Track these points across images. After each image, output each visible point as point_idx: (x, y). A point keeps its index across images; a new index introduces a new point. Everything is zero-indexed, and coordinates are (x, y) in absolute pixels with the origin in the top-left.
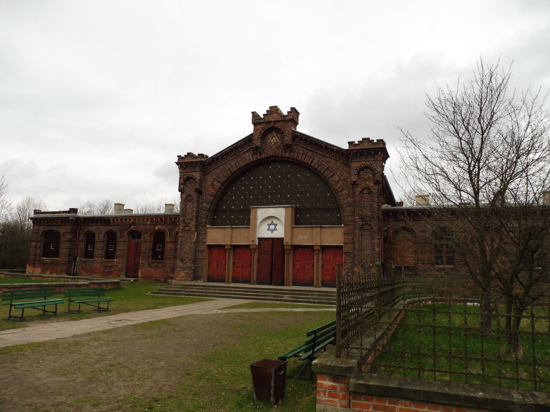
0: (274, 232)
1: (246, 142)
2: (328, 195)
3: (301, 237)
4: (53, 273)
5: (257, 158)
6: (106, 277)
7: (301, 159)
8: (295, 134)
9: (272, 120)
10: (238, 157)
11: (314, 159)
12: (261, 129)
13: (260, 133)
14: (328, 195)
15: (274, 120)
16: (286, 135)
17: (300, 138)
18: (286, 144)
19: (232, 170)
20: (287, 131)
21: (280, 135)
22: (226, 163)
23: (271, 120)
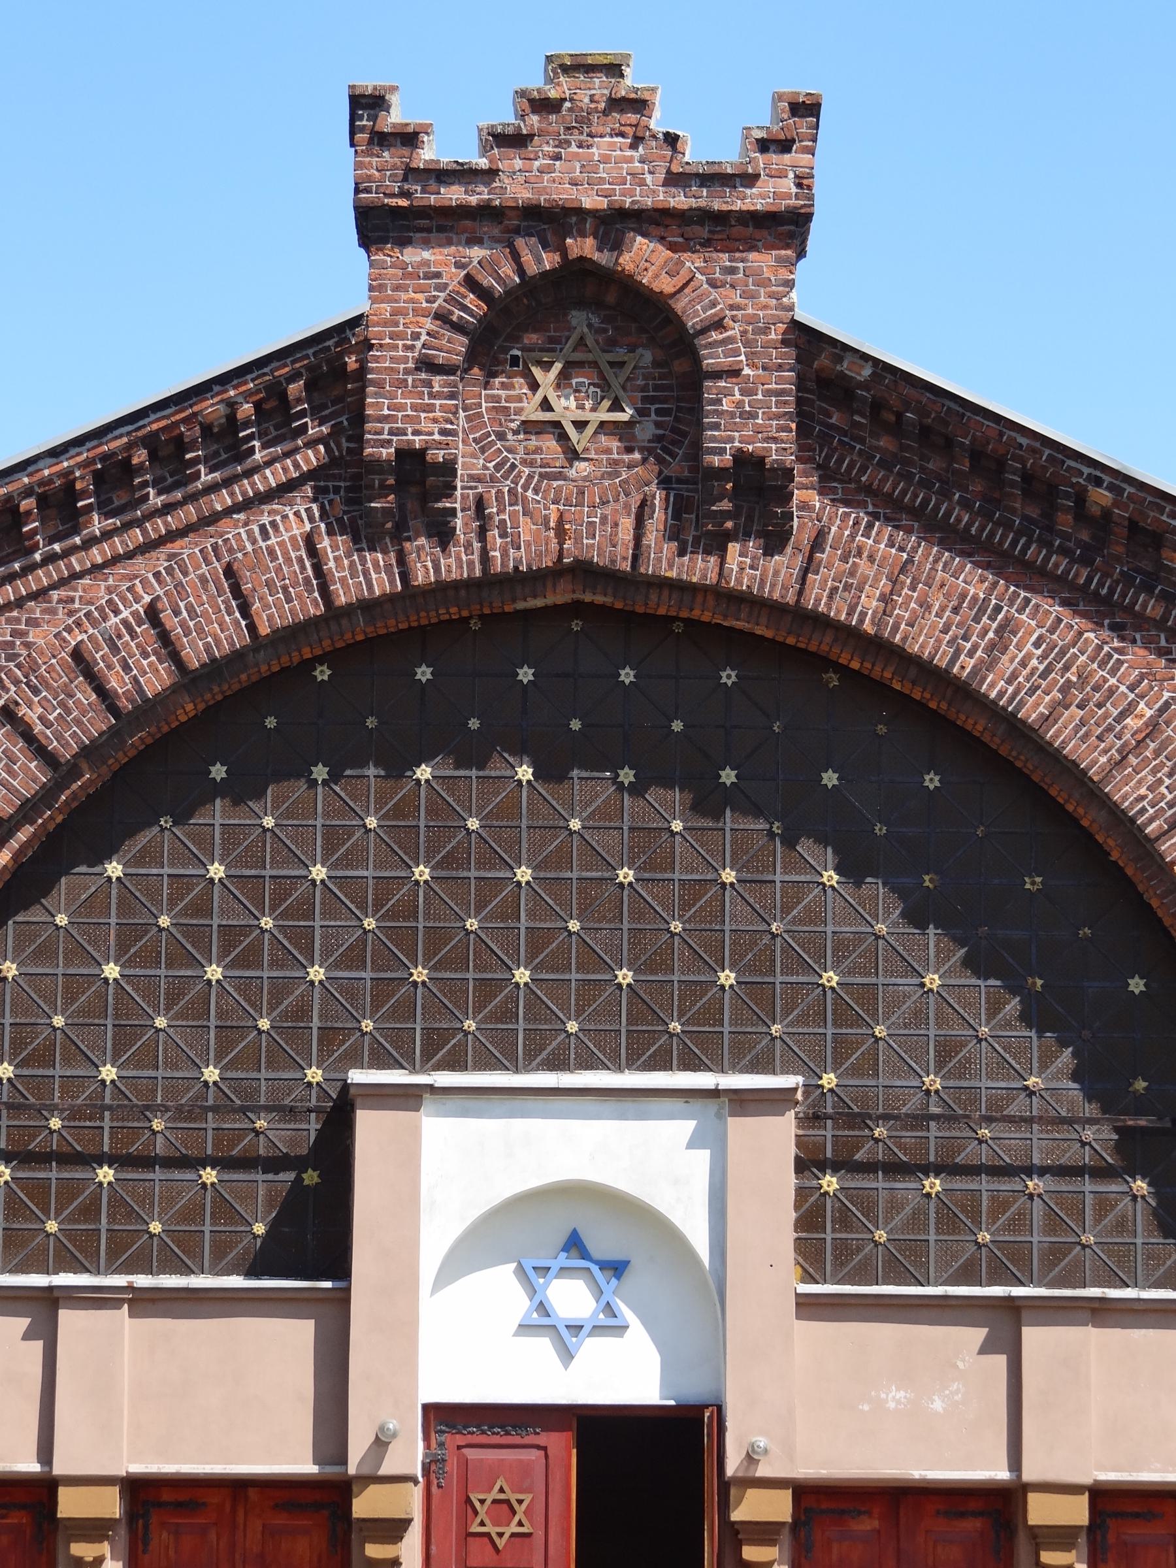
0: (591, 1348)
1: (283, 395)
2: (1137, 985)
3: (895, 1397)
4: (989, 978)
5: (405, 577)
6: (734, 380)
7: (878, 623)
8: (823, 361)
9: (588, 203)
10: (186, 548)
11: (1007, 628)
12: (453, 277)
13: (441, 317)
14: (1137, 985)
15: (602, 203)
16: (735, 373)
17: (877, 407)
18: (741, 458)
19: (117, 682)
20: (735, 331)
21: (647, 356)
22: (40, 594)
23: (564, 194)
